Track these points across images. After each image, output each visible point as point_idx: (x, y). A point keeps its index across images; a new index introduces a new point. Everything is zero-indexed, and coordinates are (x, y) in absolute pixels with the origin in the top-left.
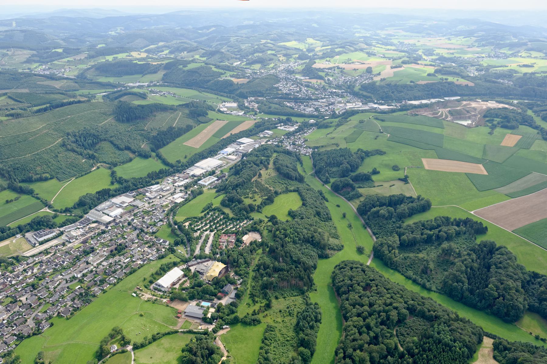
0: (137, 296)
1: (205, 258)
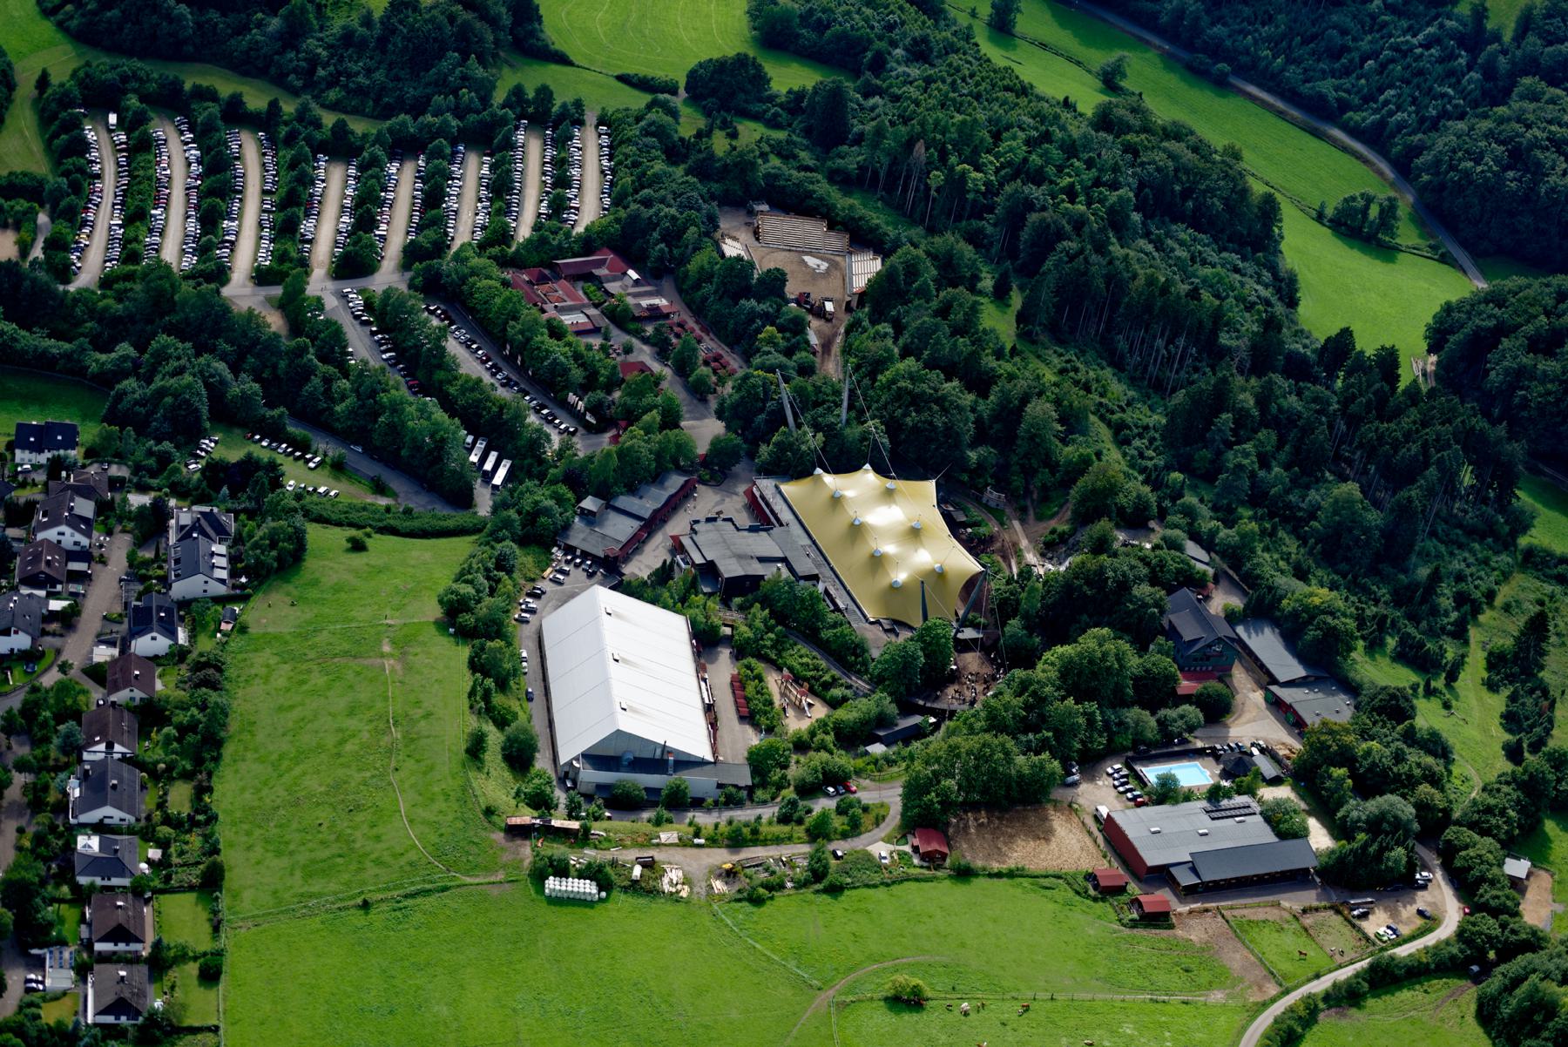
0: (604, 885)
1: (657, 478)
